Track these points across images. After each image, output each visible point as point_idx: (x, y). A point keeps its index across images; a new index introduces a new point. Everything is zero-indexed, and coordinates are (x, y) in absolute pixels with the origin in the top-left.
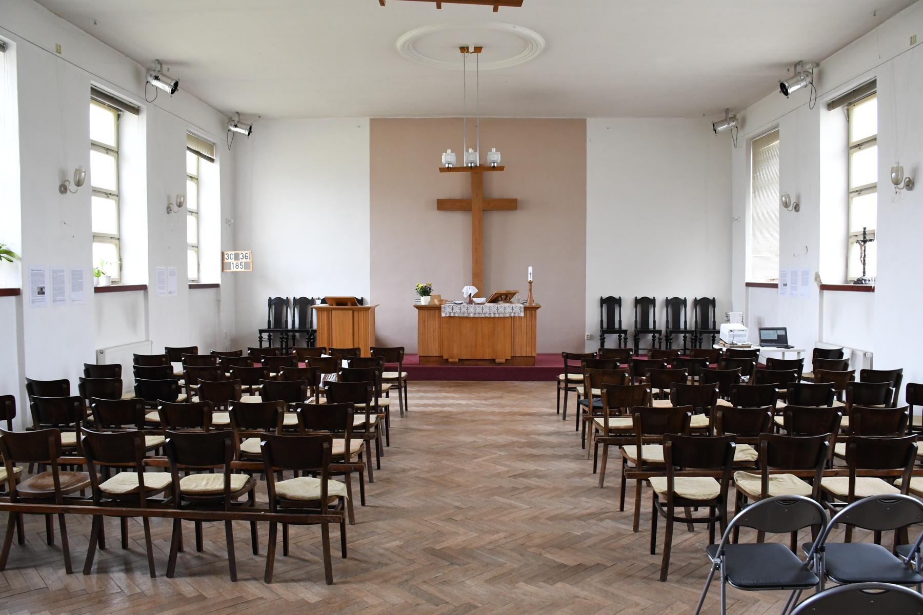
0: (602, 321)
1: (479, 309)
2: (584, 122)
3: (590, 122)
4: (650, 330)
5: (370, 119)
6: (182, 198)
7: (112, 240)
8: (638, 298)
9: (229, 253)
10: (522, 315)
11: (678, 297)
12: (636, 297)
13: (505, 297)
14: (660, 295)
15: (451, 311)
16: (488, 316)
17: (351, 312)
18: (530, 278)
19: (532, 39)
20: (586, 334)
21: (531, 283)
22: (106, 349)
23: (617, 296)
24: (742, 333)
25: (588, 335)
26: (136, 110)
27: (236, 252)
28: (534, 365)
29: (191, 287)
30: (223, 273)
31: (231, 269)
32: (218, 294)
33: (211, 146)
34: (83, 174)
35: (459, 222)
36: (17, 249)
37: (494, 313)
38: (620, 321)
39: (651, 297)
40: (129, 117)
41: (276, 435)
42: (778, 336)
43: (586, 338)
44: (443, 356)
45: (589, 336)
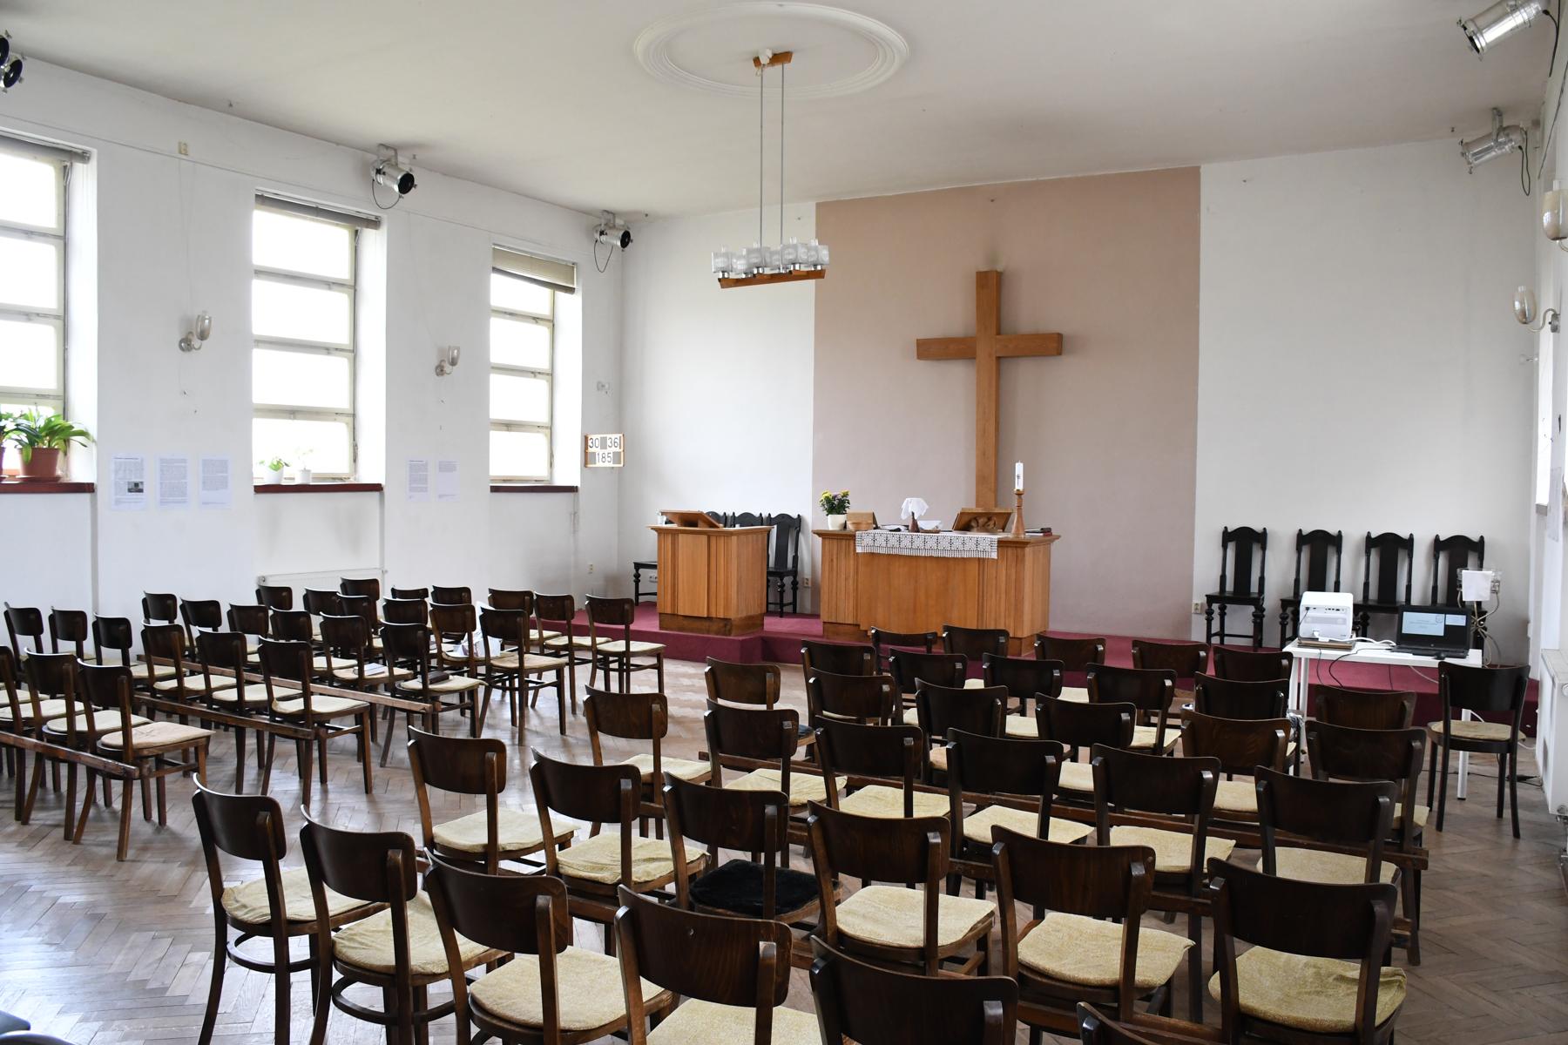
0: (1435, 588)
1: (931, 543)
2: (1191, 176)
3: (1209, 173)
4: (1398, 605)
5: (818, 205)
6: (456, 351)
7: (338, 417)
8: (1442, 539)
9: (594, 437)
10: (994, 555)
11: (779, 513)
12: (1300, 530)
13: (986, 520)
14: (1282, 530)
15: (871, 543)
16: (935, 554)
17: (704, 538)
18: (1019, 485)
19: (882, 39)
20: (1195, 601)
21: (1019, 494)
22: (271, 576)
23: (1258, 528)
24: (1337, 614)
25: (1197, 604)
26: (374, 223)
27: (602, 436)
28: (1020, 655)
29: (495, 489)
30: (585, 469)
31: (595, 463)
32: (576, 503)
33: (569, 269)
34: (207, 321)
35: (958, 379)
36: (93, 432)
37: (944, 550)
38: (1262, 579)
39: (1333, 531)
40: (369, 235)
41: (1306, 774)
42: (1447, 628)
43: (1193, 611)
44: (859, 625)
45: (1199, 607)
